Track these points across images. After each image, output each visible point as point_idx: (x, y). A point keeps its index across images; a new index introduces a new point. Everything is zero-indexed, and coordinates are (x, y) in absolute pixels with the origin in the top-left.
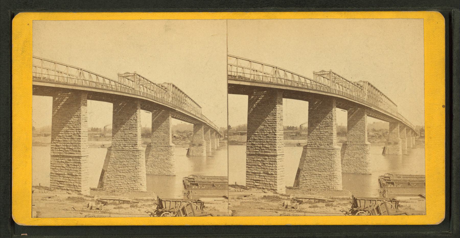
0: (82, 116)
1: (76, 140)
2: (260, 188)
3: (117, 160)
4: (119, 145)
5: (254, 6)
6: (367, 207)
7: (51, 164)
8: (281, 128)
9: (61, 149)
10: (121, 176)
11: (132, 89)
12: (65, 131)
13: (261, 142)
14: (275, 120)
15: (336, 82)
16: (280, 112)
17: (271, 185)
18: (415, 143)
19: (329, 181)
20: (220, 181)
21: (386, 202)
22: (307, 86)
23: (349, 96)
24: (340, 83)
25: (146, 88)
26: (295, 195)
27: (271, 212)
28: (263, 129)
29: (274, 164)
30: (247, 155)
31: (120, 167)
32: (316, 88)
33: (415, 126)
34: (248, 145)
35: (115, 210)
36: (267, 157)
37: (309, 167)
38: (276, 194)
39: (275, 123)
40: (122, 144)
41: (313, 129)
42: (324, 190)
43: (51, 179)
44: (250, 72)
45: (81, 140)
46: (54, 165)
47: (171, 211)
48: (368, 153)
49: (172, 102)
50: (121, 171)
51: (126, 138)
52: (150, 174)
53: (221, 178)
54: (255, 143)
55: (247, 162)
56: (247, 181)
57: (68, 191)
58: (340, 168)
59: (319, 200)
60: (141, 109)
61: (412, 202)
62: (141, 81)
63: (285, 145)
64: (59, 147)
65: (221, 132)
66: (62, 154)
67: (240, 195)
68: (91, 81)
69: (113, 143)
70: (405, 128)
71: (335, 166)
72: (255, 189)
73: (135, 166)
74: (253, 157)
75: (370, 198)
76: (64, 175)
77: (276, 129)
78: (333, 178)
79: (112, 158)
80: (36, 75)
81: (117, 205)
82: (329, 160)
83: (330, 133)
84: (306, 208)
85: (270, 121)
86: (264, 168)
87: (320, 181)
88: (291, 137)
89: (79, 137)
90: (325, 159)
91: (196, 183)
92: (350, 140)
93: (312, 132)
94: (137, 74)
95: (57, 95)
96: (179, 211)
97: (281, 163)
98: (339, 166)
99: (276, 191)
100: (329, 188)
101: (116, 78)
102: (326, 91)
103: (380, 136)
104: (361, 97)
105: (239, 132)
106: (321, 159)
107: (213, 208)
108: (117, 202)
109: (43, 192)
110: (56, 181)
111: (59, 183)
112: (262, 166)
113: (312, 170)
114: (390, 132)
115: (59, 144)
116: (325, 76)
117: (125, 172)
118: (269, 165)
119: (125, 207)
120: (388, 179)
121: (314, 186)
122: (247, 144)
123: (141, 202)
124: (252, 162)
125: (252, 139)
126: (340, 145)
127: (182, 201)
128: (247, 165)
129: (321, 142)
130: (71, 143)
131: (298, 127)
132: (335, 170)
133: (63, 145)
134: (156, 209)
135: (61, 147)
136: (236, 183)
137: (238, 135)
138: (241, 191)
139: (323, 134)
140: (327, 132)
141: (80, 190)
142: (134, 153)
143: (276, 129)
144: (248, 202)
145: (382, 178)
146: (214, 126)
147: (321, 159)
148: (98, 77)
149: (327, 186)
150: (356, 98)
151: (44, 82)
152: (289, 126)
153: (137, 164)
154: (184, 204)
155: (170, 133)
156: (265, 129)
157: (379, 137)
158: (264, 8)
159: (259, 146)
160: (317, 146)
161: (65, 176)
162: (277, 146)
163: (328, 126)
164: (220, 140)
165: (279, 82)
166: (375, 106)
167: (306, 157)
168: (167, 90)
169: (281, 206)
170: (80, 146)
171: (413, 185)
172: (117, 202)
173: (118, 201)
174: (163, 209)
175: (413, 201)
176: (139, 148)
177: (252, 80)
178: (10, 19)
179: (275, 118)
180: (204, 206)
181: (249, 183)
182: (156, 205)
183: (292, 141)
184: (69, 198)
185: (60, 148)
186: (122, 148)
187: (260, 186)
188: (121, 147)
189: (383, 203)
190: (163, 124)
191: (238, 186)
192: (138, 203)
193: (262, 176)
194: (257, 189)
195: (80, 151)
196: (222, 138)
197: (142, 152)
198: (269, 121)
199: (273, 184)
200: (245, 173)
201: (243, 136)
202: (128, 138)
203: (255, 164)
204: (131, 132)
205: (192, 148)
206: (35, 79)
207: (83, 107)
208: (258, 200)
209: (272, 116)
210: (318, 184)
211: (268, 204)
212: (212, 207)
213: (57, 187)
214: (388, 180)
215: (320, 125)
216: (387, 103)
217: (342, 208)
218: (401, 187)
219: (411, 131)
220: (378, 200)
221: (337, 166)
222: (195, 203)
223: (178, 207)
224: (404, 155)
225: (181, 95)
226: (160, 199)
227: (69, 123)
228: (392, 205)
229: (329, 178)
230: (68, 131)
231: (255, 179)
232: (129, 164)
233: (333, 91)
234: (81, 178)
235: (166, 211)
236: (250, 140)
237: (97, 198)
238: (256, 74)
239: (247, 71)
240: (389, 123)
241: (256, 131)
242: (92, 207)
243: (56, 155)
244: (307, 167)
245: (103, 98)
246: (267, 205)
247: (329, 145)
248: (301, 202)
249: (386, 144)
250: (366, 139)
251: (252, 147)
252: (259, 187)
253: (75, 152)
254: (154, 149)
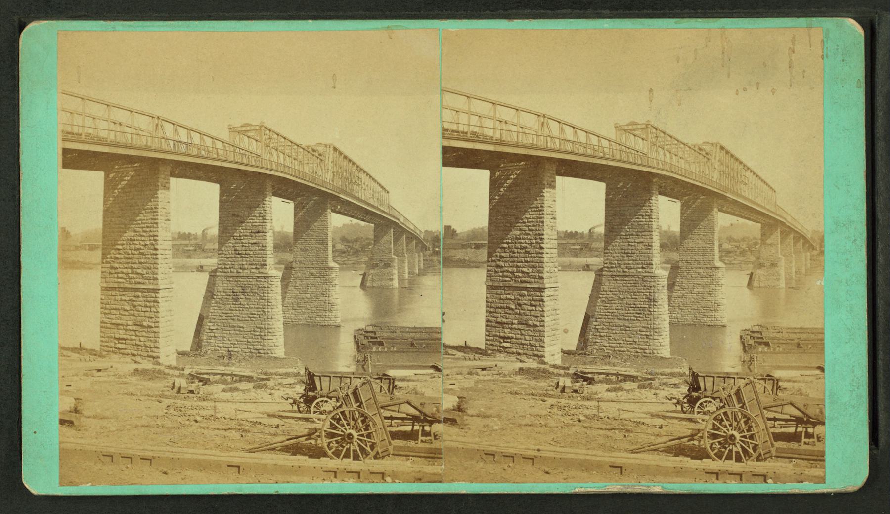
0: (159, 210)
1: (535, 255)
2: (513, 353)
3: (227, 295)
4: (617, 265)
6: (718, 391)
7: (102, 303)
8: (552, 235)
9: (120, 275)
10: (234, 327)
11: (641, 154)
12: (128, 240)
13: (514, 262)
14: (155, 221)
15: (272, 145)
16: (551, 202)
17: (534, 348)
18: (424, 265)
19: (646, 340)
20: (425, 336)
21: (755, 380)
22: (604, 154)
23: (683, 172)
24: (666, 147)
25: (284, 154)
26: (195, 367)
27: (150, 402)
28: (132, 238)
29: (540, 306)
30: (487, 288)
31: (232, 310)
32: (621, 156)
33: (423, 231)
34: (489, 268)
35: (609, 394)
36: (526, 292)
37: (221, 312)
38: (542, 364)
39: (541, 224)
40: (623, 263)
41: (228, 238)
42: (635, 356)
43: (102, 334)
44: (495, 124)
45: (159, 256)
46: (108, 306)
47: (331, 395)
48: (720, 283)
49: (333, 181)
50: (622, 317)
51: (630, 251)
52: (677, 322)
53: (427, 330)
54: (502, 264)
55: (487, 302)
56: (102, 341)
57: (134, 358)
58: (665, 313)
59: (626, 376)
60: (274, 195)
61: (804, 381)
62: (659, 139)
63: (560, 268)
64: (116, 271)
65: (427, 241)
66: (122, 285)
67: (473, 366)
68: (177, 141)
69: (219, 263)
70: (792, 236)
71: (270, 310)
72: (502, 355)
73: (261, 307)
74: (499, 291)
75: (340, 373)
76: (127, 325)
77: (543, 237)
78: (652, 333)
79: (604, 291)
80: (72, 129)
81: (227, 384)
82: (644, 297)
83: (647, 244)
84: (216, 393)
85: (532, 222)
86: (520, 314)
87: (628, 339)
88: (185, 253)
89: (154, 252)
90: (637, 297)
91: (765, 340)
92: (685, 259)
93: (613, 244)
94: (265, 128)
95: (113, 167)
96: (347, 395)
97: (552, 303)
98: (278, 310)
99: (158, 359)
100: (645, 353)
101: (225, 135)
102: (640, 162)
103: (744, 250)
104: (320, 175)
105: (471, 241)
106: (629, 296)
107: (413, 390)
108: (229, 378)
109: (88, 359)
110: (111, 337)
111: (117, 342)
112: (516, 309)
113: (611, 317)
114: (375, 244)
115: (116, 265)
116: (637, 133)
117: (242, 320)
118: (529, 308)
119: (628, 388)
120: (759, 335)
121: (616, 349)
122: (488, 266)
123: (274, 379)
124: (498, 302)
125: (111, 258)
126: (665, 269)
127: (352, 376)
128: (487, 307)
129: (630, 262)
130: (140, 263)
131: (585, 232)
132: (270, 317)
133: (125, 266)
134: (687, 393)
135: (506, 269)
136: (466, 343)
137: (471, 248)
138: (92, 359)
139: (633, 247)
140: (255, 243)
141: (542, 353)
142: (647, 281)
143: (157, 238)
144: (489, 380)
145: (747, 334)
146: (412, 228)
147: (629, 296)
148: (576, 132)
149: (256, 350)
150: (311, 177)
151: (473, 141)
152: (568, 232)
153: (266, 304)
154: (357, 382)
155: (329, 243)
156: (521, 236)
157: (354, 253)
158: (510, 12)
159: (510, 270)
160: (621, 270)
161: (128, 327)
162: (546, 269)
163: (643, 232)
164: (424, 256)
165: (549, 145)
166: (733, 192)
167: (601, 292)
168: (324, 159)
169: (167, 389)
170: (157, 269)
171: (806, 348)
172: (229, 378)
173: (229, 377)
174: (699, 392)
175: (421, 377)
176: (270, 272)
177: (497, 140)
179: (155, 217)
180: (396, 386)
181: (106, 344)
182: (303, 385)
183: (575, 260)
184: (136, 370)
185: (118, 273)
186: (624, 272)
187: (512, 349)
188: (235, 271)
189: (366, 381)
190: (315, 224)
191: (470, 348)
192: (268, 379)
193: (515, 329)
194: (506, 354)
195: (543, 278)
196: (428, 252)
197: (274, 280)
198: (144, 222)
199: (152, 346)
200: (484, 323)
201: (480, 250)
202: (247, 252)
203: (502, 305)
204: (255, 241)
205: (759, 271)
206: (68, 136)
207: (163, 191)
208: (508, 376)
209: (535, 211)
210: (624, 345)
211: (528, 385)
212: (796, 388)
213: (114, 349)
214: (758, 338)
215: (628, 230)
216: (756, 185)
217: (285, 393)
218: (397, 352)
219: (414, 242)
220: (738, 376)
222: (378, 381)
223: (346, 389)
224: (789, 288)
225: (736, 167)
226: (310, 373)
227: (521, 221)
228: (381, 387)
229: (644, 333)
230: (134, 240)
231: (502, 334)
232: (249, 303)
233: (267, 163)
234: (159, 332)
235: (322, 396)
236: (494, 259)
237: (191, 370)
238: (119, 130)
239: (489, 123)
240: (759, 225)
241: (505, 241)
242: (180, 389)
243: (496, 284)
244: (602, 311)
245: (201, 174)
246: (527, 386)
247: (644, 268)
248: (206, 382)
249: (368, 266)
250: (330, 257)
251: (112, 274)
252: (510, 351)
253: (147, 281)
254: (299, 274)
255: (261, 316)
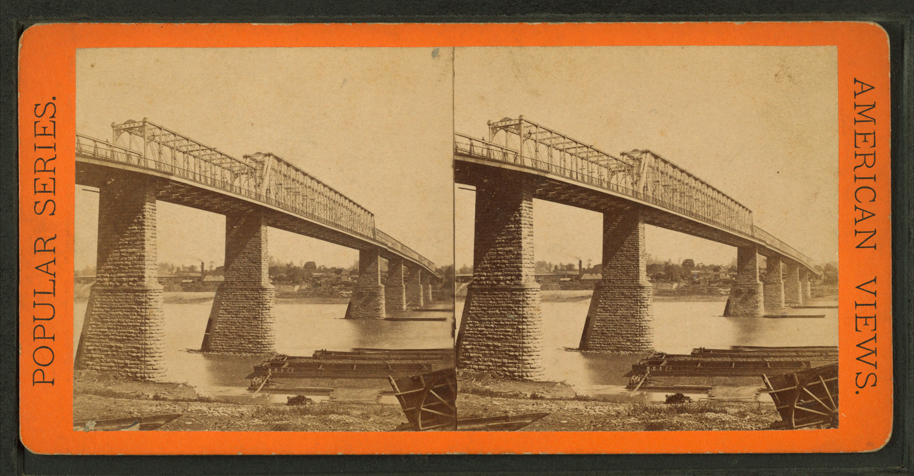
3: (482, 310)
5: (508, 11)
18: (812, 294)
106: (121, 313)
116: (570, 151)
139: (126, 259)
158: (527, 15)
167: (471, 308)
178: (15, 38)
196: (818, 282)
221: (152, 328)
255: (138, 335)
